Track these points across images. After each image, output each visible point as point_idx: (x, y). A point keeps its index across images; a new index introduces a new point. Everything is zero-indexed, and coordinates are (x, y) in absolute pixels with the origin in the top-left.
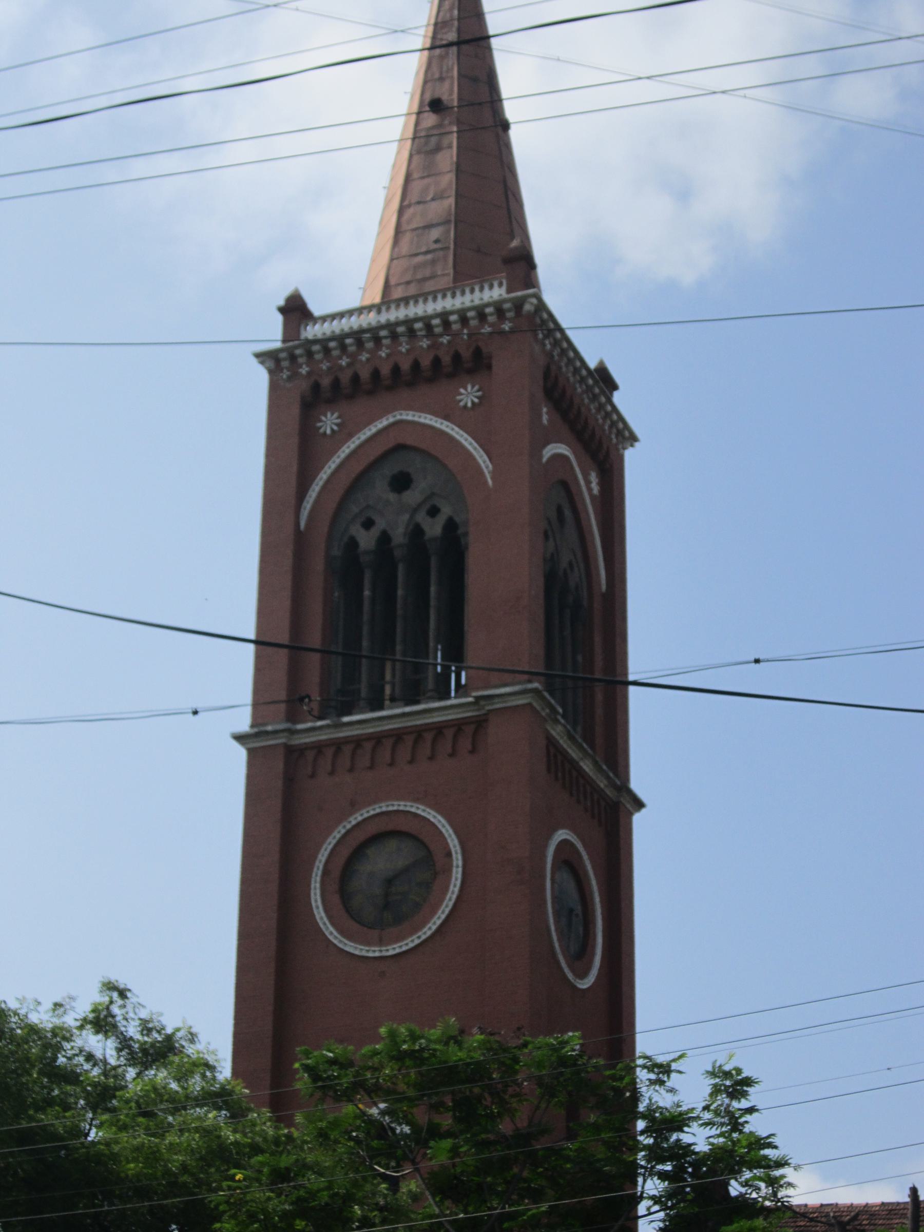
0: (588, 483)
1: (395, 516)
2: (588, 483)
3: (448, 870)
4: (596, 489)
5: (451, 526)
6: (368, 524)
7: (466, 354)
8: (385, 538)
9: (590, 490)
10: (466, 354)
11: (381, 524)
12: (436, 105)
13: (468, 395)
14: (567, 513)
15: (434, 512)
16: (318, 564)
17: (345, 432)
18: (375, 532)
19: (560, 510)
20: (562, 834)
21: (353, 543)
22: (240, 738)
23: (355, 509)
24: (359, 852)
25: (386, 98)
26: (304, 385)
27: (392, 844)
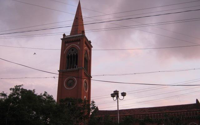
5: (77, 54)
8: (71, 55)
13: (79, 43)
22: (61, 39)
24: (68, 81)
27: (71, 80)
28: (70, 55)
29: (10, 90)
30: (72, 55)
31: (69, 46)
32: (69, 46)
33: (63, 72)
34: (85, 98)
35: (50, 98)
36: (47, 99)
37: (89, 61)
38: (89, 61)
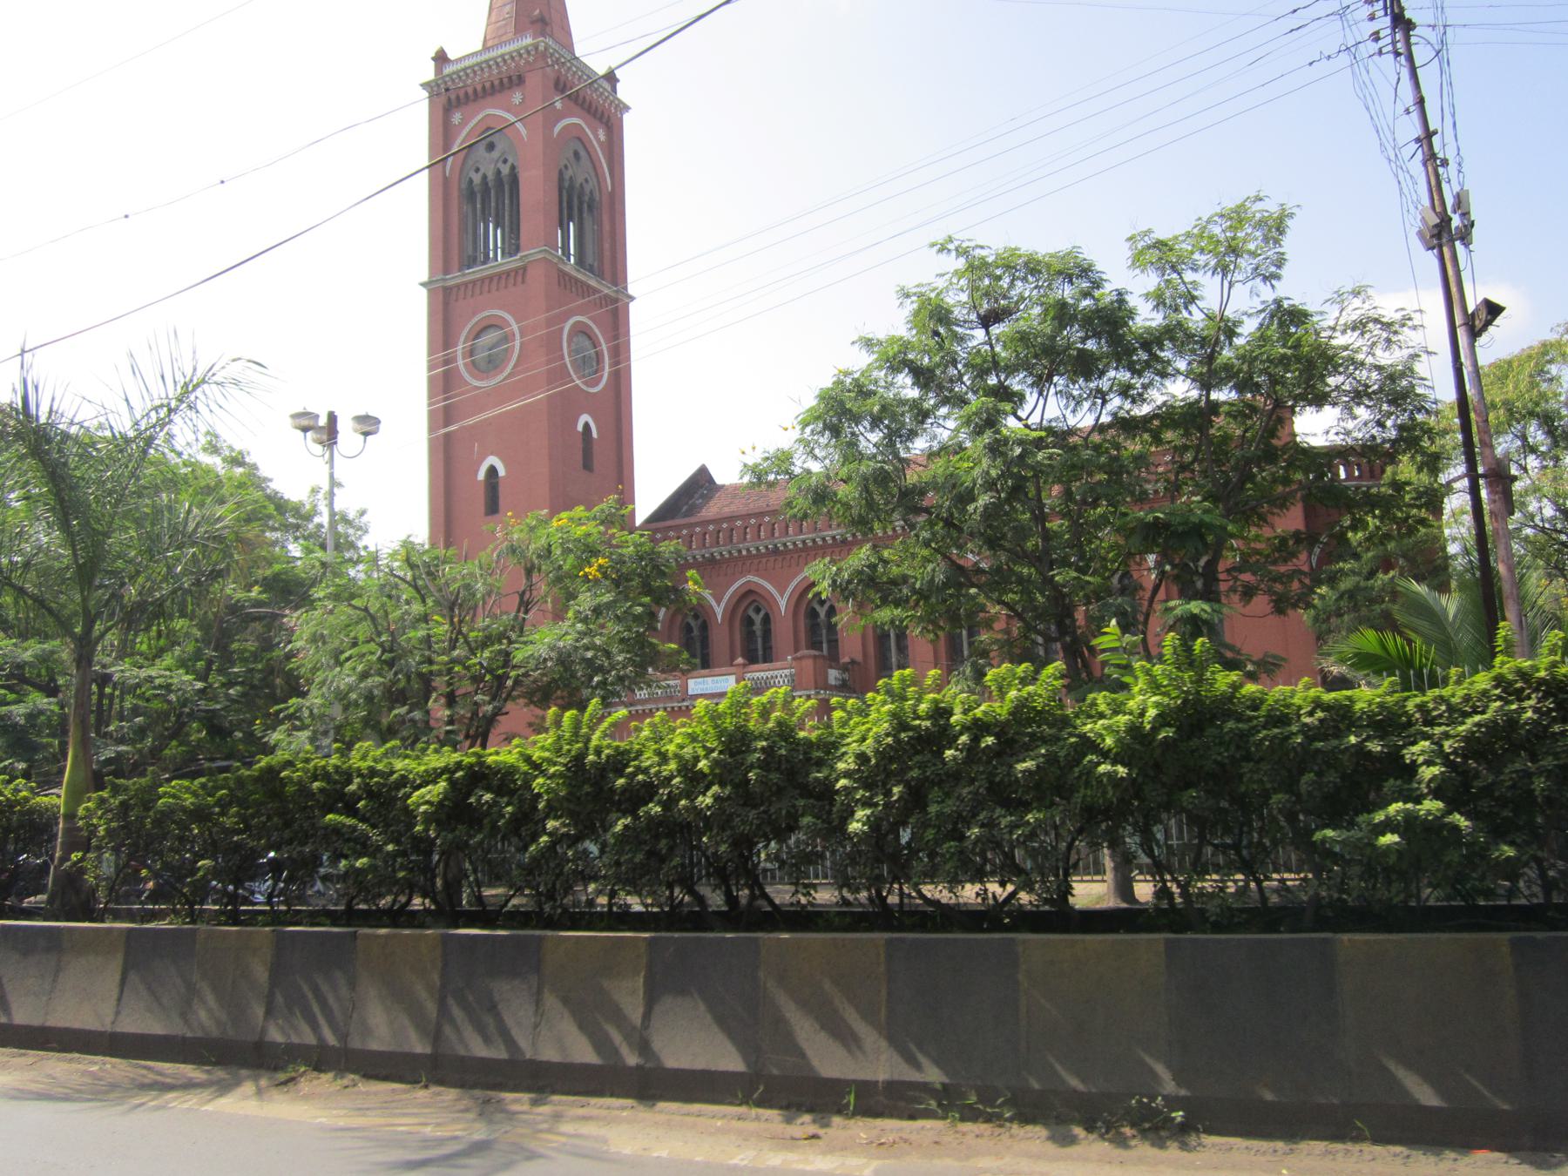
2: (596, 136)
5: (513, 168)
8: (485, 177)
13: (517, 98)
14: (583, 153)
28: (477, 178)
29: (1496, 299)
31: (468, 125)
32: (468, 125)
33: (447, 291)
34: (587, 425)
37: (605, 199)
38: (605, 199)
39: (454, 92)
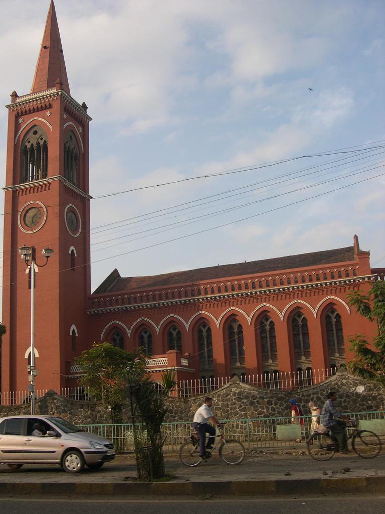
0: (78, 130)
1: (33, 140)
2: (78, 130)
3: (43, 215)
4: (81, 131)
5: (45, 142)
6: (29, 142)
7: (47, 105)
8: (38, 107)
9: (79, 131)
10: (47, 105)
11: (31, 142)
12: (45, 47)
13: (48, 113)
14: (73, 137)
15: (42, 139)
16: (19, 151)
17: (24, 122)
18: (30, 144)
19: (71, 136)
20: (69, 206)
21: (26, 146)
22: (8, 106)
23: (26, 139)
24: (27, 211)
25: (36, 37)
26: (15, 113)
27: (34, 209)
30: (35, 145)
34: (73, 251)
35: (150, 358)
36: (185, 362)
37: (81, 156)
39: (19, 111)
